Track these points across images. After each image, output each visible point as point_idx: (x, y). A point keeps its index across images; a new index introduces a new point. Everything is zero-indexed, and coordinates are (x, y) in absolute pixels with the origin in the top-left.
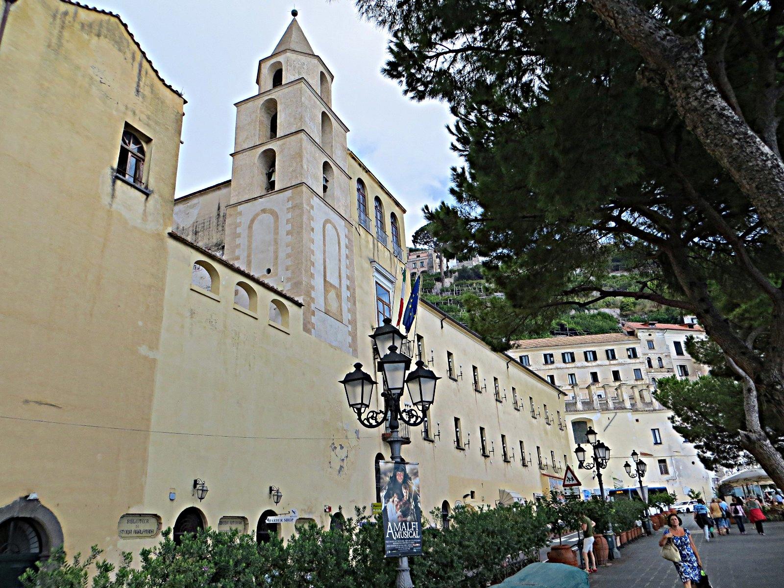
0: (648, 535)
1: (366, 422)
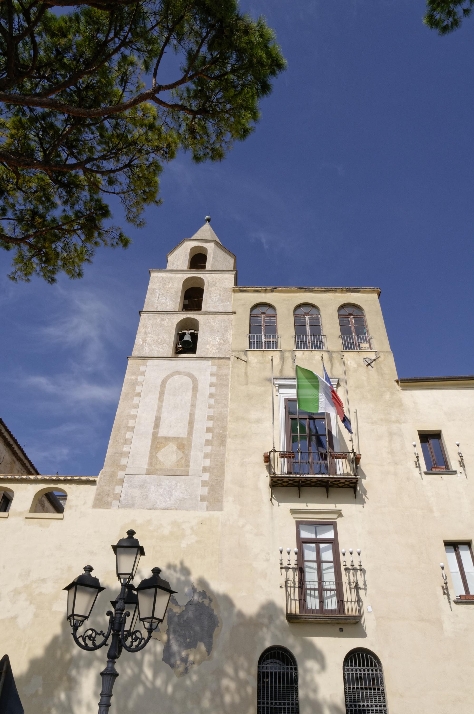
0: (213, 158)
1: (81, 640)
